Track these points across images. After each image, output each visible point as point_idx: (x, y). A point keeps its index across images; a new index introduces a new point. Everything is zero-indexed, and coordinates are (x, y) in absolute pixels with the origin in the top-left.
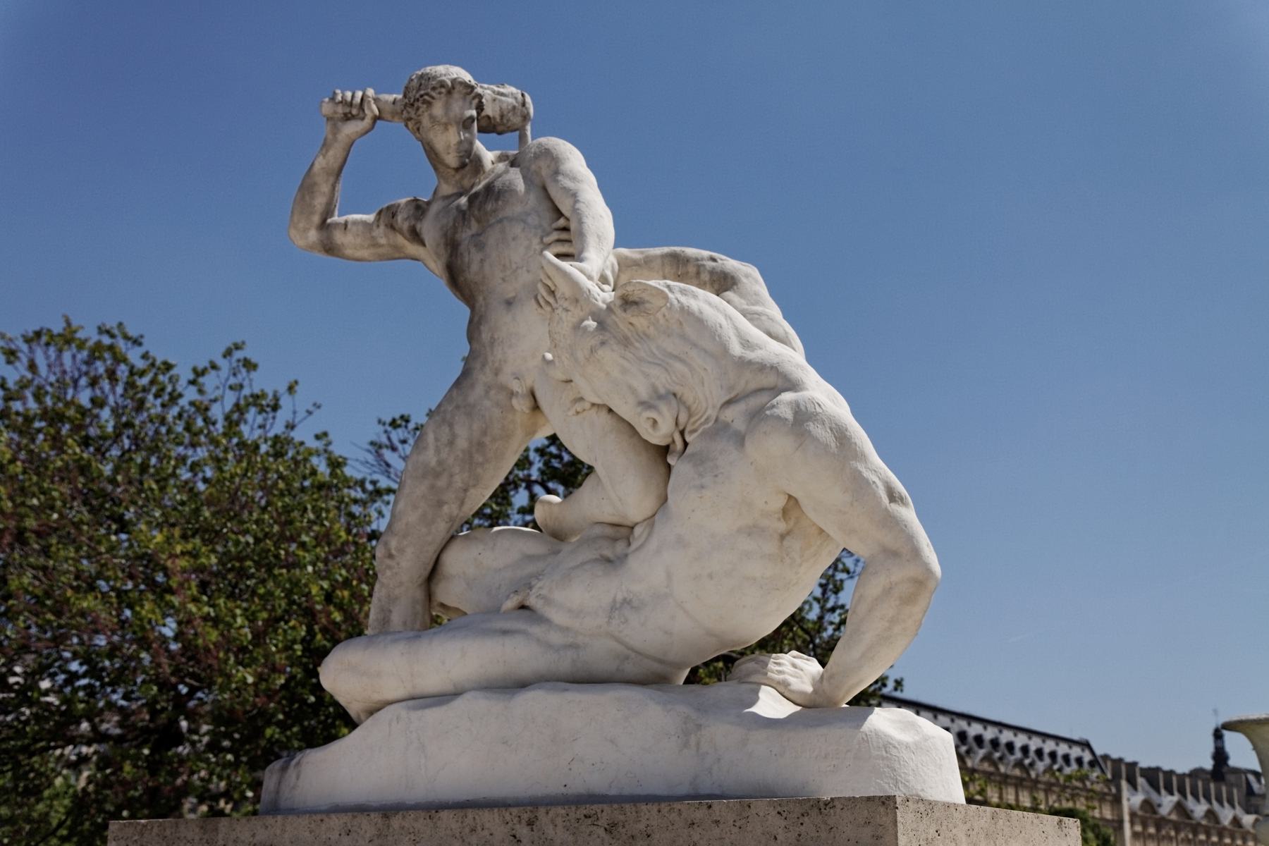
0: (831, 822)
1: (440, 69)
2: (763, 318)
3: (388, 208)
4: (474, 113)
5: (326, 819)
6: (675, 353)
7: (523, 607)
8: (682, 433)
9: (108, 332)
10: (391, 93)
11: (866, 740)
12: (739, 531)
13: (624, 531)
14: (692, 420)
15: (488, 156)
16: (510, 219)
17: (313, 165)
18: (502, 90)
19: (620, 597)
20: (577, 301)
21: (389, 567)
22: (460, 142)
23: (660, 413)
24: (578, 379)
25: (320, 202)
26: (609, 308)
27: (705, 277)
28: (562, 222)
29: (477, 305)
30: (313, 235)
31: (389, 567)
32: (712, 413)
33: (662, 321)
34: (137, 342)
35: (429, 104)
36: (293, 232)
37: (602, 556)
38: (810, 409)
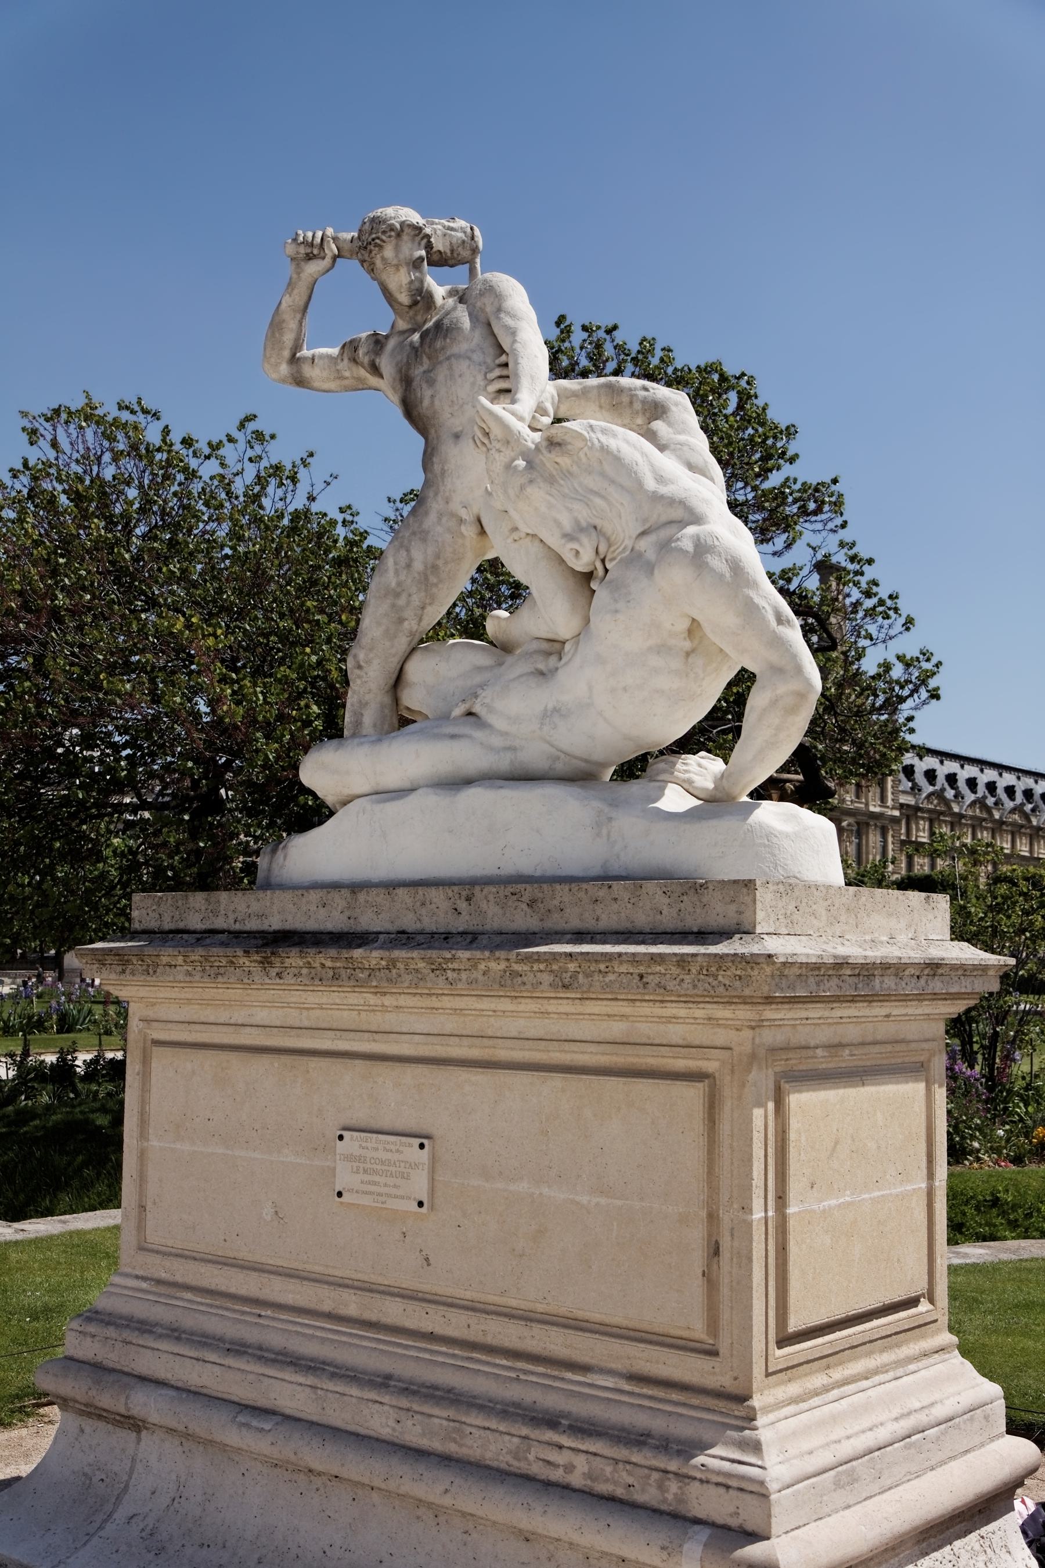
0: (705, 900)
1: (389, 211)
2: (685, 448)
3: (351, 342)
4: (423, 253)
5: (306, 894)
6: (595, 489)
7: (470, 714)
8: (603, 561)
9: (127, 408)
10: (348, 231)
11: (751, 830)
12: (650, 649)
13: (557, 646)
14: (612, 549)
15: (439, 292)
16: (458, 356)
17: (280, 303)
18: (451, 225)
19: (550, 706)
20: (508, 442)
21: (359, 677)
22: (411, 282)
23: (581, 545)
24: (512, 513)
25: (288, 338)
26: (537, 448)
27: (638, 406)
28: (503, 358)
29: (430, 437)
30: (284, 369)
31: (359, 677)
32: (629, 543)
33: (584, 460)
34: (156, 416)
35: (381, 247)
36: (267, 366)
37: (536, 670)
38: (710, 542)
